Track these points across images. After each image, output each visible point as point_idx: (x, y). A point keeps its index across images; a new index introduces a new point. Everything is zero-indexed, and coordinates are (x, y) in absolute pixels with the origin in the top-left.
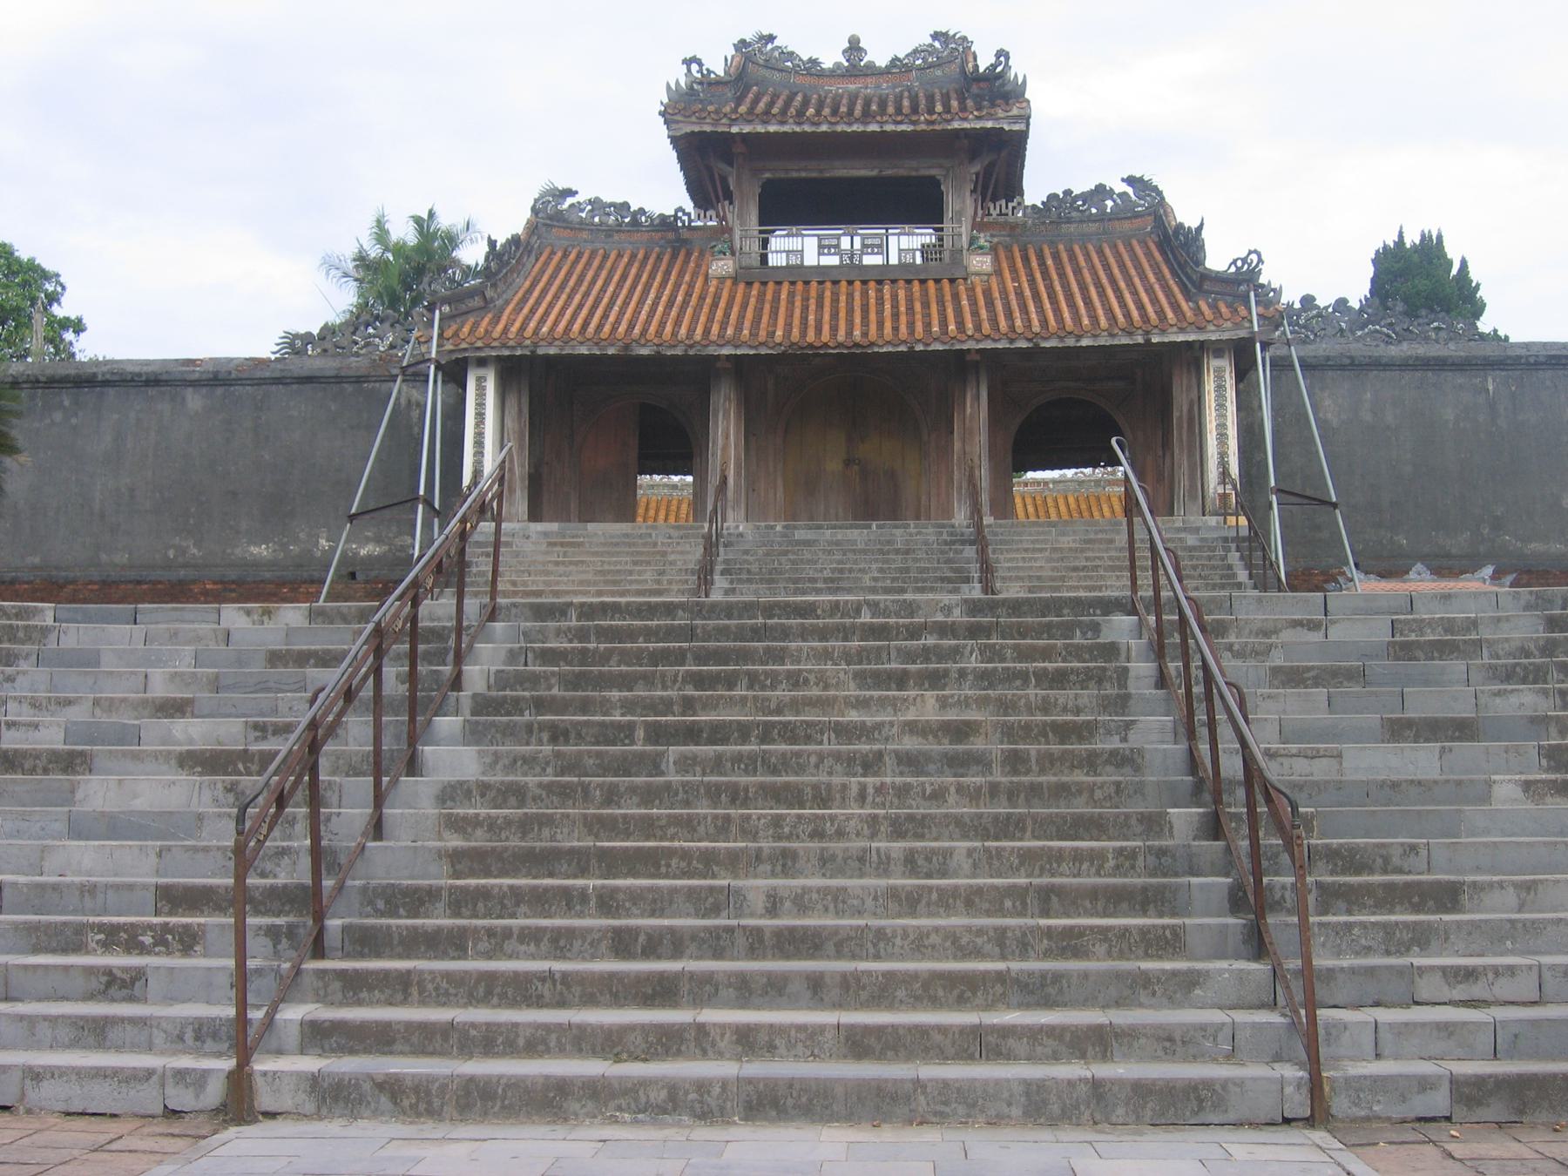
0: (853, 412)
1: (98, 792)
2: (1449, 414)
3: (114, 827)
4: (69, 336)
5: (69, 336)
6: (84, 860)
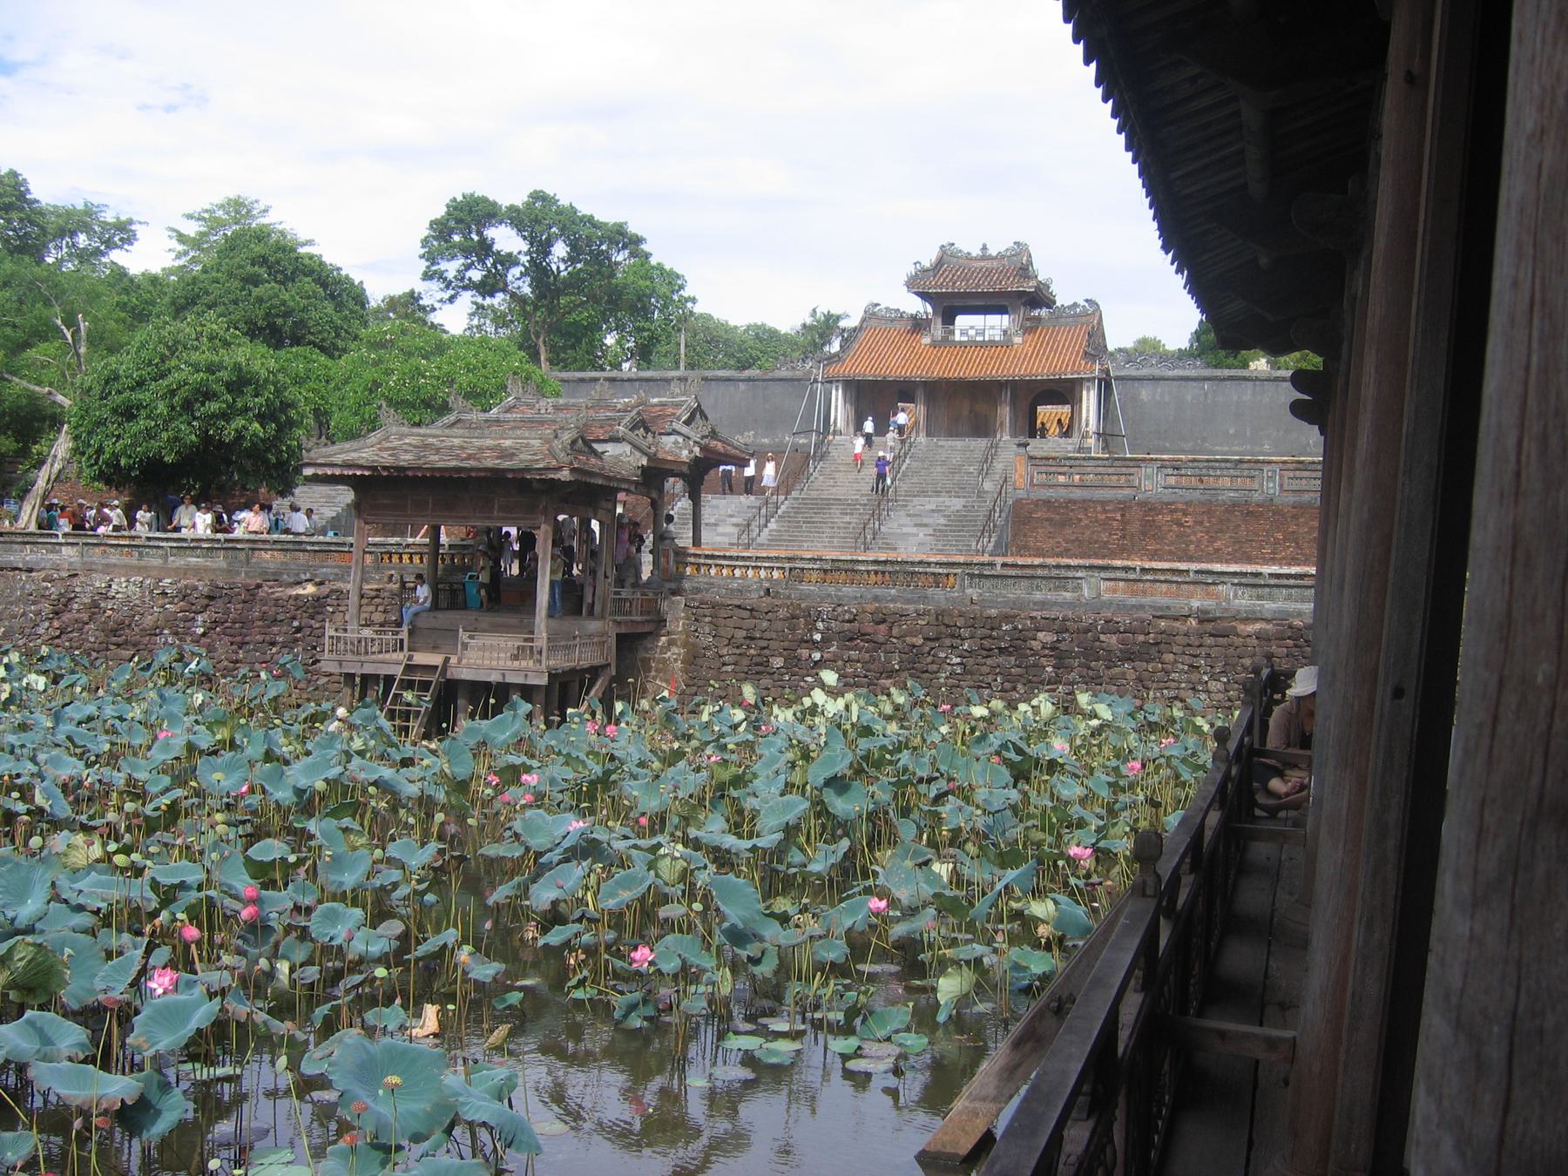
0: (965, 404)
1: (720, 530)
2: (1189, 398)
3: (723, 535)
6: (719, 539)
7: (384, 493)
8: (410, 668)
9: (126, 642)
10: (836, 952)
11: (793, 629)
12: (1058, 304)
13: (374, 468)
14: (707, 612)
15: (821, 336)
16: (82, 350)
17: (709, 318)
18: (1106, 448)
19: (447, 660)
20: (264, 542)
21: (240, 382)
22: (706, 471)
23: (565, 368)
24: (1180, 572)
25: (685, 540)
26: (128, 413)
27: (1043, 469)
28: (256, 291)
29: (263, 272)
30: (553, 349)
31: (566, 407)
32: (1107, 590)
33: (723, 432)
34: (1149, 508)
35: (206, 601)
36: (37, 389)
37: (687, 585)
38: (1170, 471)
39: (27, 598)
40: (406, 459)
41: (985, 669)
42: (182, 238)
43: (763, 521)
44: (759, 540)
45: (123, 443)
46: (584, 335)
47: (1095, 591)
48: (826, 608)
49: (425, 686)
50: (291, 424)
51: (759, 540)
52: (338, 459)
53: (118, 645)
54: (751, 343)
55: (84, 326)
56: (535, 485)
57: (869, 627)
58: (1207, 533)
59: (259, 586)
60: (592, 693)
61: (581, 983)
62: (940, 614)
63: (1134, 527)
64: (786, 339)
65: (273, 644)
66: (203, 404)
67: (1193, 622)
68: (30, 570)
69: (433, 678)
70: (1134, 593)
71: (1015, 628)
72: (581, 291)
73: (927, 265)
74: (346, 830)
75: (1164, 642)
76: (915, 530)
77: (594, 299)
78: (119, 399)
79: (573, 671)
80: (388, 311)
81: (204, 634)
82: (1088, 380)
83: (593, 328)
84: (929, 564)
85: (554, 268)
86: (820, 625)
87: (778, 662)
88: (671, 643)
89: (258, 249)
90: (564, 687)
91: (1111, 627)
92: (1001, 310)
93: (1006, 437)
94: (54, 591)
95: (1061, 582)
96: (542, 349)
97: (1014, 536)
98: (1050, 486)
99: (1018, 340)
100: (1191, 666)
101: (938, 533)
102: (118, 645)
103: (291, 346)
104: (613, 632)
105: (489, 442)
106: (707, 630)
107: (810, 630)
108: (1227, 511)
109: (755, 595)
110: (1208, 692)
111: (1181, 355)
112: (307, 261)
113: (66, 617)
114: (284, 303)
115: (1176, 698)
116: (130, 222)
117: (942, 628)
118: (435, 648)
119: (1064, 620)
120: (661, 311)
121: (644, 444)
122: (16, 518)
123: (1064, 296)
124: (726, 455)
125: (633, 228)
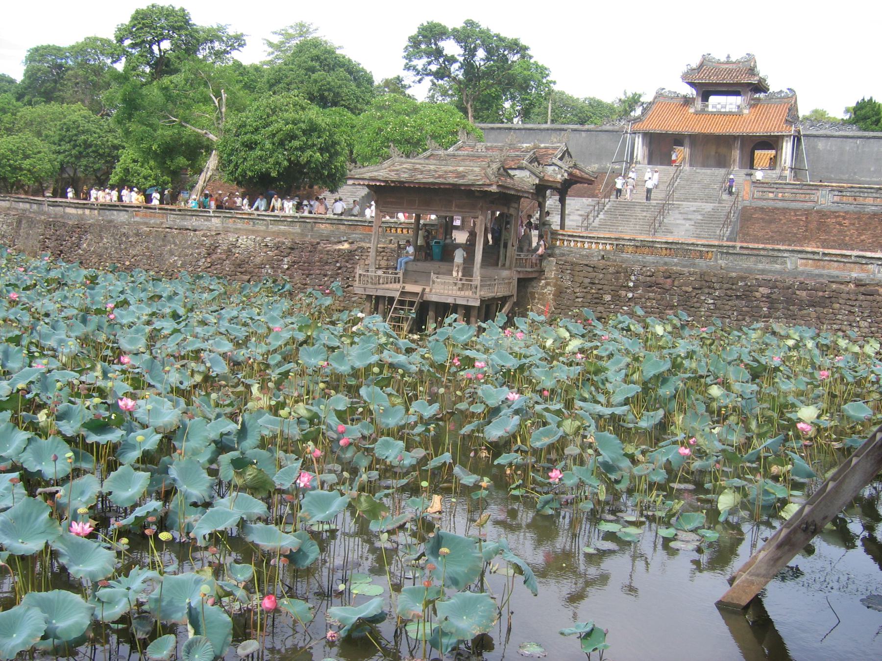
0: (714, 148)
2: (848, 148)
3: (573, 221)
4: (552, 85)
5: (552, 85)
7: (387, 194)
8: (403, 293)
9: (246, 272)
10: (660, 477)
11: (617, 279)
12: (771, 91)
13: (386, 182)
14: (569, 267)
15: (630, 107)
16: (224, 110)
17: (563, 93)
18: (796, 177)
19: (424, 289)
20: (322, 219)
21: (312, 129)
22: (569, 187)
23: (483, 121)
24: (846, 256)
25: (556, 226)
26: (250, 146)
27: (760, 189)
28: (314, 76)
29: (316, 64)
30: (475, 110)
31: (492, 148)
32: (801, 265)
33: (581, 165)
34: (822, 214)
35: (289, 251)
36: (200, 131)
37: (557, 251)
38: (836, 193)
39: (193, 246)
40: (404, 177)
41: (727, 307)
42: (271, 44)
43: (596, 213)
44: (594, 224)
45: (251, 163)
46: (493, 102)
47: (795, 264)
48: (637, 268)
49: (412, 304)
50: (337, 154)
51: (594, 224)
52: (367, 176)
53: (241, 273)
54: (587, 108)
55: (224, 96)
56: (477, 194)
57: (661, 280)
58: (857, 230)
59: (318, 243)
60: (503, 311)
61: (518, 487)
62: (702, 275)
63: (813, 226)
64: (611, 109)
65: (325, 275)
66: (290, 142)
67: (852, 286)
68: (195, 230)
69: (417, 300)
70: (817, 267)
71: (746, 285)
72: (493, 79)
73: (694, 66)
74: (389, 395)
75: (834, 296)
76: (683, 222)
77: (500, 83)
78: (246, 138)
79: (494, 299)
80: (385, 87)
81: (288, 269)
82: (787, 136)
83: (498, 98)
84: (697, 245)
85: (478, 64)
86: (633, 278)
87: (608, 298)
88: (547, 284)
89: (315, 52)
90: (488, 307)
91: (803, 286)
92: (737, 93)
93: (737, 168)
94: (208, 242)
95: (774, 259)
96: (470, 111)
97: (742, 227)
98: (764, 199)
99: (746, 111)
100: (850, 311)
101: (697, 224)
102: (241, 273)
103: (332, 106)
104: (516, 277)
105: (451, 168)
106: (568, 277)
107: (627, 280)
108: (870, 218)
109: (595, 259)
110: (859, 327)
111: (844, 122)
112: (341, 59)
113: (214, 257)
114: (329, 83)
115: (839, 330)
116: (242, 35)
117: (704, 283)
118: (416, 282)
119: (776, 281)
120: (536, 89)
121: (537, 171)
122: (187, 202)
123: (774, 86)
124: (582, 178)
125: (523, 42)
